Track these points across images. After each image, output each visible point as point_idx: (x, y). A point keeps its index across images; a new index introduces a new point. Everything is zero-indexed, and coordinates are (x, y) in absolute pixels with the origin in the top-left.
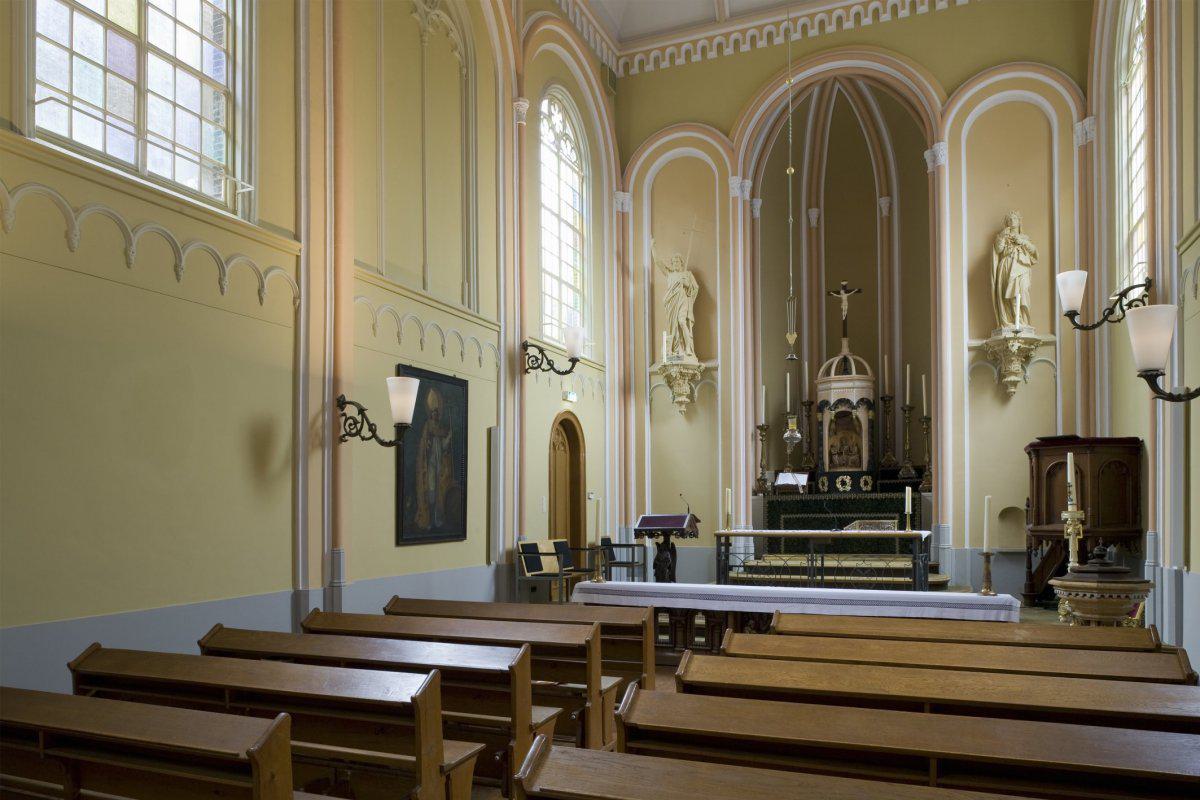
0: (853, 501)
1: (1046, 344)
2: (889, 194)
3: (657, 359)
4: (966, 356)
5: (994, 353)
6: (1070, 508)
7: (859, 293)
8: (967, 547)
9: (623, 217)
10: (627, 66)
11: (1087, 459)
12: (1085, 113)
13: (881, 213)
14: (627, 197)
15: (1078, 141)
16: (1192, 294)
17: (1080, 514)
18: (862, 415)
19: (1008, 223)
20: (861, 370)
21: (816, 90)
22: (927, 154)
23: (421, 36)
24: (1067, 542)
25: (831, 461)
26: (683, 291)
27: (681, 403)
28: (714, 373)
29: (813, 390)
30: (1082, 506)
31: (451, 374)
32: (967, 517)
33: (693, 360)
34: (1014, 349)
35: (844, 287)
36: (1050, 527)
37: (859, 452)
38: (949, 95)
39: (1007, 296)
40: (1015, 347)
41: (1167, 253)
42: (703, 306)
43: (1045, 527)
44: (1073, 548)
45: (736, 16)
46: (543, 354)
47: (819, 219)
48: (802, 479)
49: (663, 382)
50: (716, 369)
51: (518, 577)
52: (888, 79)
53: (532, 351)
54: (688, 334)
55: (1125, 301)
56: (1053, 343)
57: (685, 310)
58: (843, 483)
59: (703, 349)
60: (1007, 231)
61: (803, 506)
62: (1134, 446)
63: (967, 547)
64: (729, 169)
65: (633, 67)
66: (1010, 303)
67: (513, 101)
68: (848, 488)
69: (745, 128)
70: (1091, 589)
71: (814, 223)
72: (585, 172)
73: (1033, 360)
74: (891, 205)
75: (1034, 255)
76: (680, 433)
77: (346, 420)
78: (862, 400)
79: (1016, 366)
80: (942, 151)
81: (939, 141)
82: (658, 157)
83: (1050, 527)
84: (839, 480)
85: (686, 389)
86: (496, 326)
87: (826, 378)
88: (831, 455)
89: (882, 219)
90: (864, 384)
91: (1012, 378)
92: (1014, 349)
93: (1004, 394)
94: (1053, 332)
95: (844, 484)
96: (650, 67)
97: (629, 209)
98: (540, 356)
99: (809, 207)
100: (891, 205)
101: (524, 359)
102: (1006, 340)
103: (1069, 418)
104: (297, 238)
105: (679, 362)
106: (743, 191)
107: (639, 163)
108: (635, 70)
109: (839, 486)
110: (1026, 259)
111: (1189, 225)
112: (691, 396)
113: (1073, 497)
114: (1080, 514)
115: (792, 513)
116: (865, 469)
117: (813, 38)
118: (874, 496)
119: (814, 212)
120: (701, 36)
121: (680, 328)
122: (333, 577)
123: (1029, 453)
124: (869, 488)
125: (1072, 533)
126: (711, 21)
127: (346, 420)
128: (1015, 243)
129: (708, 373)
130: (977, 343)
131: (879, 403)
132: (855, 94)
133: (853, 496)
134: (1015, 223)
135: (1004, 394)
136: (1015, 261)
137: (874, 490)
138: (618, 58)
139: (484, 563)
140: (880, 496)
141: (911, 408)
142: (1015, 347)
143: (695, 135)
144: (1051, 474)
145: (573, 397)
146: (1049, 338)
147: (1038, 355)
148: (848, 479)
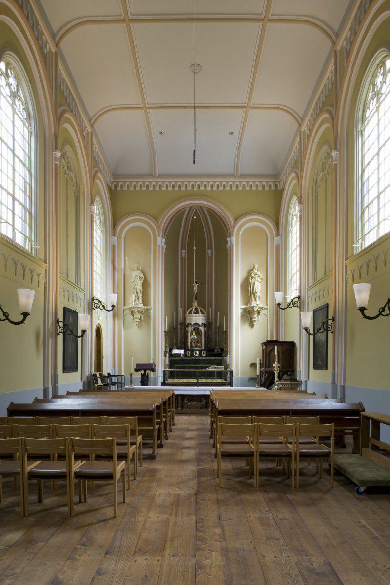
0: (184, 360)
1: (265, 309)
2: (211, 248)
3: (126, 303)
4: (240, 311)
5: (249, 311)
6: (276, 363)
7: (202, 284)
8: (239, 376)
9: (114, 246)
10: (115, 186)
11: (281, 347)
12: (278, 235)
13: (208, 255)
14: (116, 238)
15: (275, 243)
16: (311, 303)
17: (279, 365)
18: (202, 329)
19: (254, 267)
20: (202, 313)
21: (188, 209)
22: (228, 239)
23: (67, 182)
24: (275, 373)
25: (191, 345)
26: (139, 278)
27: (136, 322)
28: (150, 311)
29: (184, 319)
30: (279, 362)
31: (74, 310)
32: (240, 367)
33: (142, 305)
34: (256, 310)
35: (196, 282)
36: (269, 369)
37: (201, 342)
38: (236, 220)
39: (254, 292)
40: (256, 309)
41: (304, 290)
42: (146, 284)
43: (268, 369)
44: (276, 375)
45: (160, 176)
46: (101, 303)
47: (185, 254)
48: (182, 352)
49: (130, 313)
50: (150, 309)
51: (92, 386)
52: (216, 211)
53: (96, 301)
54: (140, 295)
55: (293, 302)
56: (267, 309)
57: (139, 287)
58: (196, 353)
59: (146, 301)
60: (254, 270)
61: (183, 361)
62: (293, 344)
63: (239, 376)
64: (157, 234)
65: (118, 187)
66: (254, 294)
67: (89, 205)
68: (198, 355)
69: (164, 218)
70: (287, 384)
71: (183, 256)
72: (102, 229)
73: (261, 314)
74: (212, 253)
75: (262, 279)
76: (135, 334)
77: (60, 328)
78: (203, 323)
79: (256, 315)
80: (234, 239)
81: (233, 236)
82: (130, 223)
83: (269, 369)
84: (194, 352)
85: (139, 316)
86: (83, 291)
87: (189, 315)
88: (191, 343)
89: (208, 257)
90: (204, 318)
91: (254, 319)
92: (256, 310)
93: (252, 325)
94: (267, 305)
95: (196, 354)
96: (125, 188)
97: (116, 244)
98: (99, 304)
99: (182, 249)
100: (212, 253)
101: (93, 304)
102: (253, 307)
103: (272, 335)
104: (45, 262)
105: (137, 306)
106: (162, 243)
107: (119, 228)
108: (119, 188)
109: (194, 354)
110: (260, 280)
111: (310, 284)
112: (140, 319)
113: (277, 359)
114: (279, 365)
115: (179, 364)
116: (203, 348)
117: (188, 190)
118: (206, 358)
119: (184, 252)
120: (147, 181)
121: (137, 293)
122: (55, 382)
123: (262, 345)
124: (205, 355)
125: (276, 370)
126: (151, 176)
127: (60, 328)
128: (256, 274)
129: (148, 311)
130: (244, 307)
131: (207, 325)
132: (202, 212)
133: (199, 358)
134: (256, 267)
135: (252, 325)
136: (256, 281)
137: (206, 356)
138: (112, 182)
139: (80, 381)
140: (208, 358)
141: (219, 327)
142: (256, 309)
143: (144, 218)
144: (270, 352)
145: (101, 318)
146: (266, 307)
147: (263, 312)
148: (198, 352)
